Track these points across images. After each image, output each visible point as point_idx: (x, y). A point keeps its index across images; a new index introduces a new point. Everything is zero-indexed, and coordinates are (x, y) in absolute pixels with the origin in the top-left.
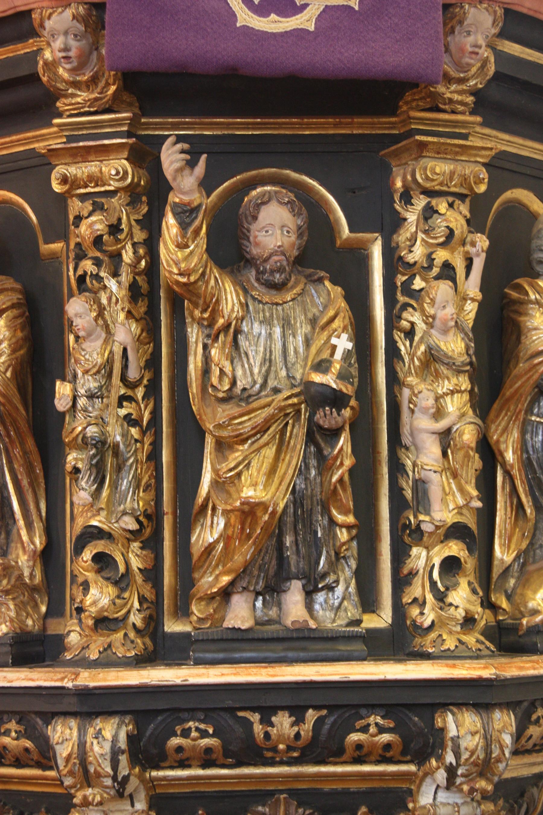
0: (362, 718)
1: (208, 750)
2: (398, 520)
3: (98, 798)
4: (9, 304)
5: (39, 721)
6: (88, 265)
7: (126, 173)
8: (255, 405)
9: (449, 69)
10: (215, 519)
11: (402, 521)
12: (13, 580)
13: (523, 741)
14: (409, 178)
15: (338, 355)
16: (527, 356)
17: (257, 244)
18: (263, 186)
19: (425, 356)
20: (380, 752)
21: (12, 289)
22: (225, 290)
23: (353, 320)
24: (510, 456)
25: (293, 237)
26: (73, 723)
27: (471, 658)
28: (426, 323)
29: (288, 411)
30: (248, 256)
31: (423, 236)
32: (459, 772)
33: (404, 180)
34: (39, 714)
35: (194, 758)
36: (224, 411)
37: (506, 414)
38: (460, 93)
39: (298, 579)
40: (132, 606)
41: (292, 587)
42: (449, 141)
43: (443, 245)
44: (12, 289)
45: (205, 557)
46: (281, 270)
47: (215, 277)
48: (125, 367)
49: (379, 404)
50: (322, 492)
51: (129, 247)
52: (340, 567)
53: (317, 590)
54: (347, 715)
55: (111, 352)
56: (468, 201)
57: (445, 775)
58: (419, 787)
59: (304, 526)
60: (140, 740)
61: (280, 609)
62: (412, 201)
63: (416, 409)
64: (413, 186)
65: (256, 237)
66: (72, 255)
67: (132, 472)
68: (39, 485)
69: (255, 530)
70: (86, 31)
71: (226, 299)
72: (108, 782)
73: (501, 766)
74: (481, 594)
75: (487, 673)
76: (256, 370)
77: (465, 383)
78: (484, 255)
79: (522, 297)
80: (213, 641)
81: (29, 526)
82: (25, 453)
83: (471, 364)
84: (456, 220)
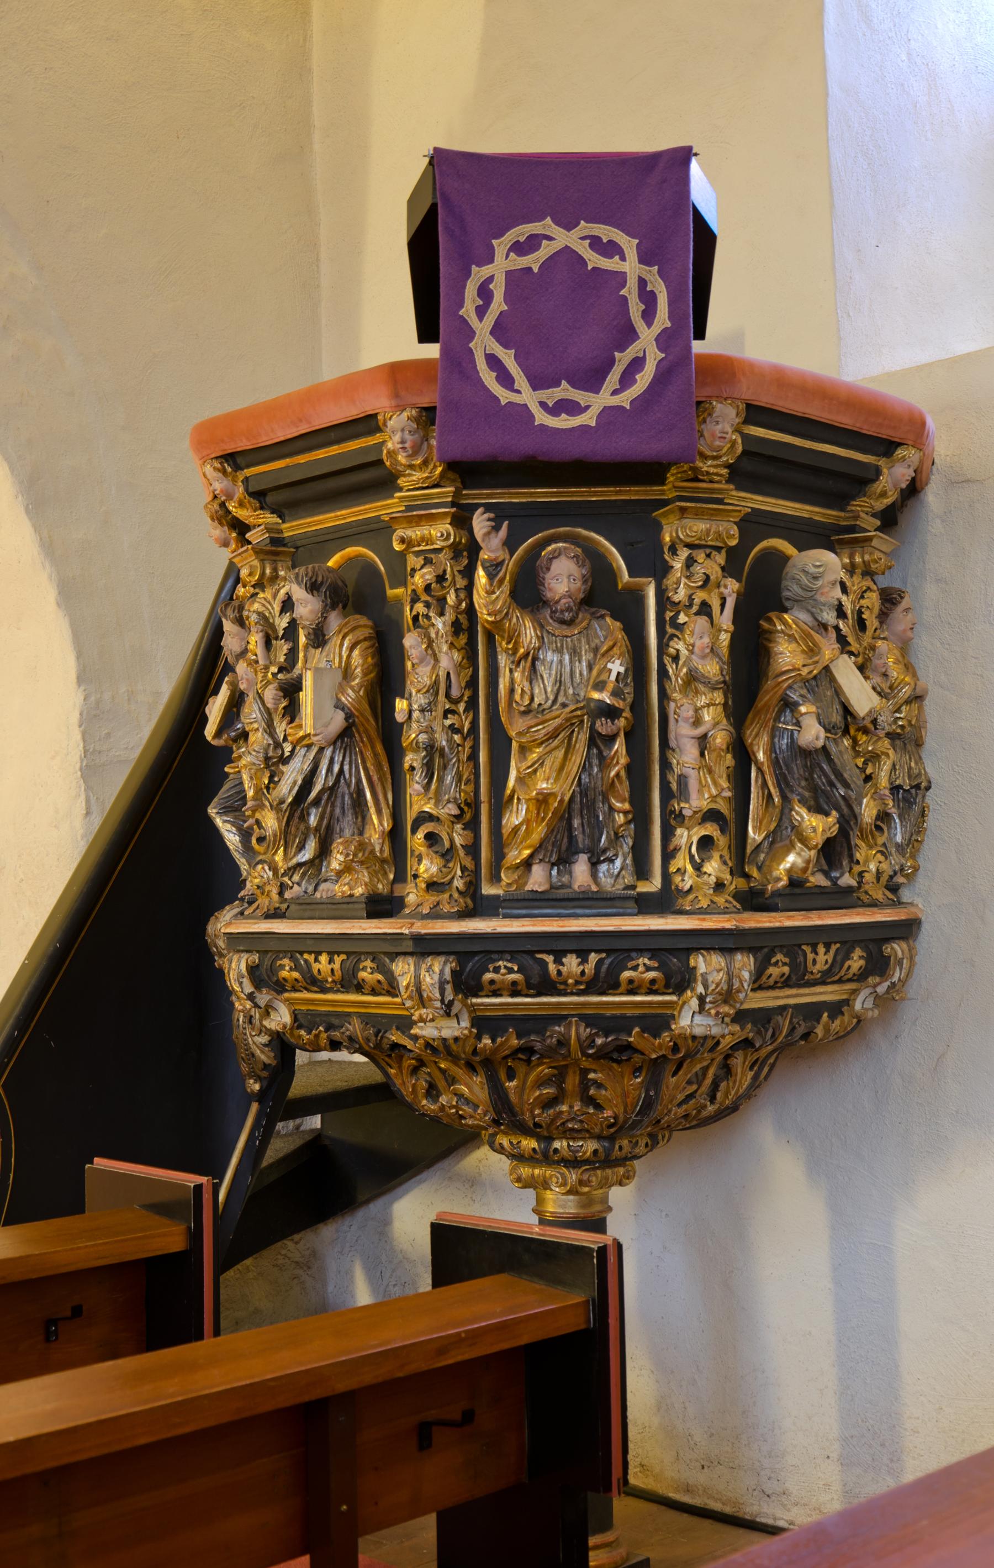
0: (633, 960)
1: (514, 983)
2: (666, 807)
3: (430, 1016)
4: (362, 637)
5: (387, 961)
6: (420, 608)
7: (449, 535)
8: (548, 717)
9: (704, 450)
10: (520, 806)
11: (669, 808)
12: (366, 854)
13: (764, 979)
14: (674, 534)
15: (613, 677)
16: (773, 676)
17: (550, 590)
18: (556, 543)
19: (687, 677)
20: (648, 985)
21: (365, 626)
22: (525, 626)
23: (630, 648)
24: (761, 756)
25: (579, 584)
26: (411, 960)
27: (719, 913)
28: (688, 650)
29: (574, 721)
30: (545, 599)
31: (686, 581)
32: (708, 1000)
33: (671, 536)
34: (385, 953)
35: (504, 989)
36: (524, 722)
37: (758, 723)
38: (716, 466)
39: (584, 853)
40: (455, 873)
41: (580, 859)
42: (704, 506)
43: (702, 587)
44: (365, 626)
45: (513, 835)
46: (569, 609)
47: (517, 616)
48: (449, 687)
49: (653, 715)
50: (602, 785)
51: (452, 591)
52: (619, 844)
53: (600, 862)
54: (621, 957)
55: (438, 676)
56: (724, 551)
57: (697, 1002)
58: (680, 1012)
59: (588, 811)
60: (461, 975)
61: (571, 877)
62: (678, 552)
63: (679, 719)
64: (678, 541)
65: (549, 584)
66: (409, 600)
67: (455, 770)
68: (386, 779)
69: (548, 814)
70: (418, 428)
71: (526, 633)
72: (438, 1004)
73: (742, 996)
74: (730, 864)
75: (728, 925)
76: (549, 689)
77: (719, 697)
78: (735, 595)
79: (771, 627)
80: (518, 900)
81: (379, 812)
82: (376, 755)
83: (724, 682)
84: (712, 568)
